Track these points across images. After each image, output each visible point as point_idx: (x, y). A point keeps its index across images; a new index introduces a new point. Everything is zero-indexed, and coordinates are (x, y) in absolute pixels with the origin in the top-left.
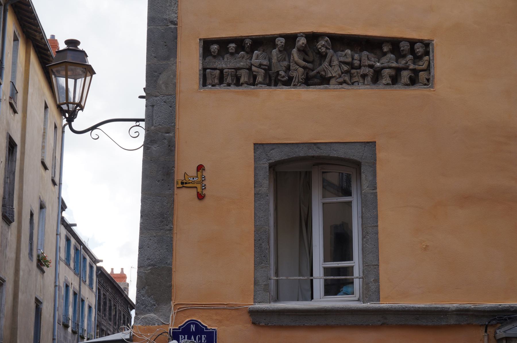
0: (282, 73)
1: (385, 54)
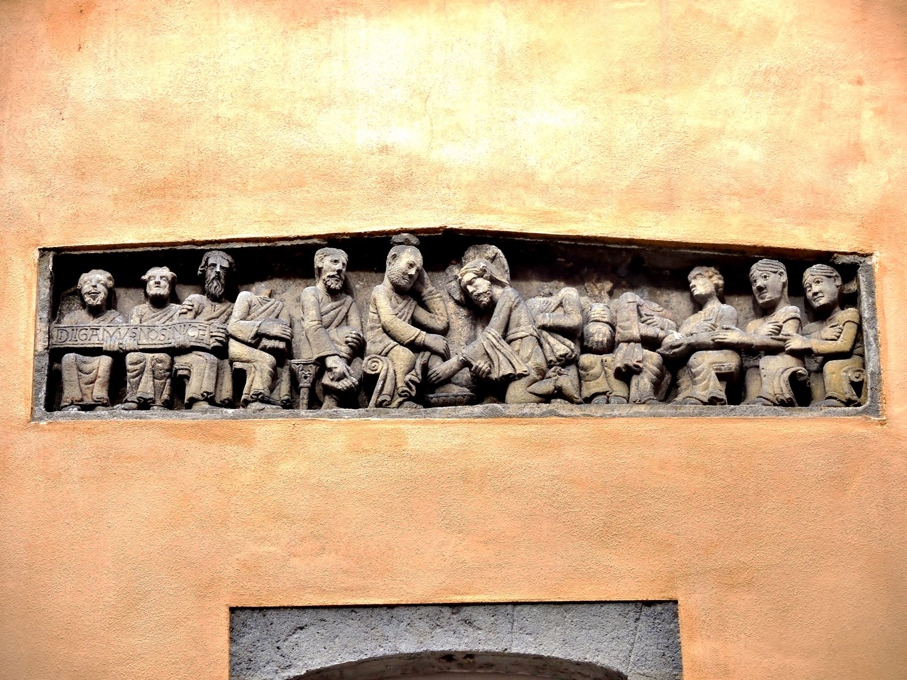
0: (336, 364)
1: (698, 303)
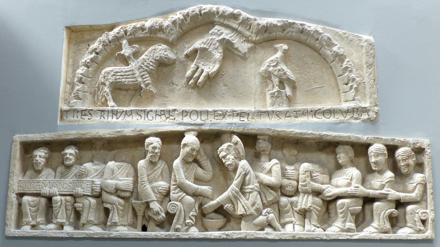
0: (155, 206)
